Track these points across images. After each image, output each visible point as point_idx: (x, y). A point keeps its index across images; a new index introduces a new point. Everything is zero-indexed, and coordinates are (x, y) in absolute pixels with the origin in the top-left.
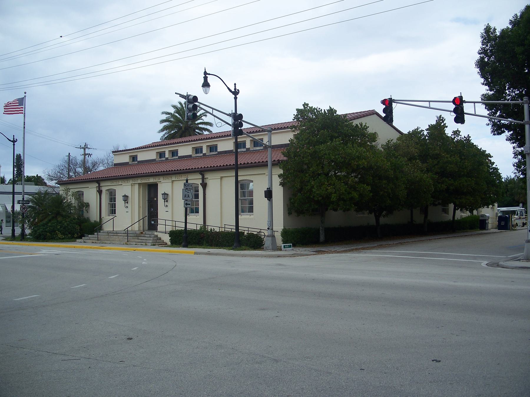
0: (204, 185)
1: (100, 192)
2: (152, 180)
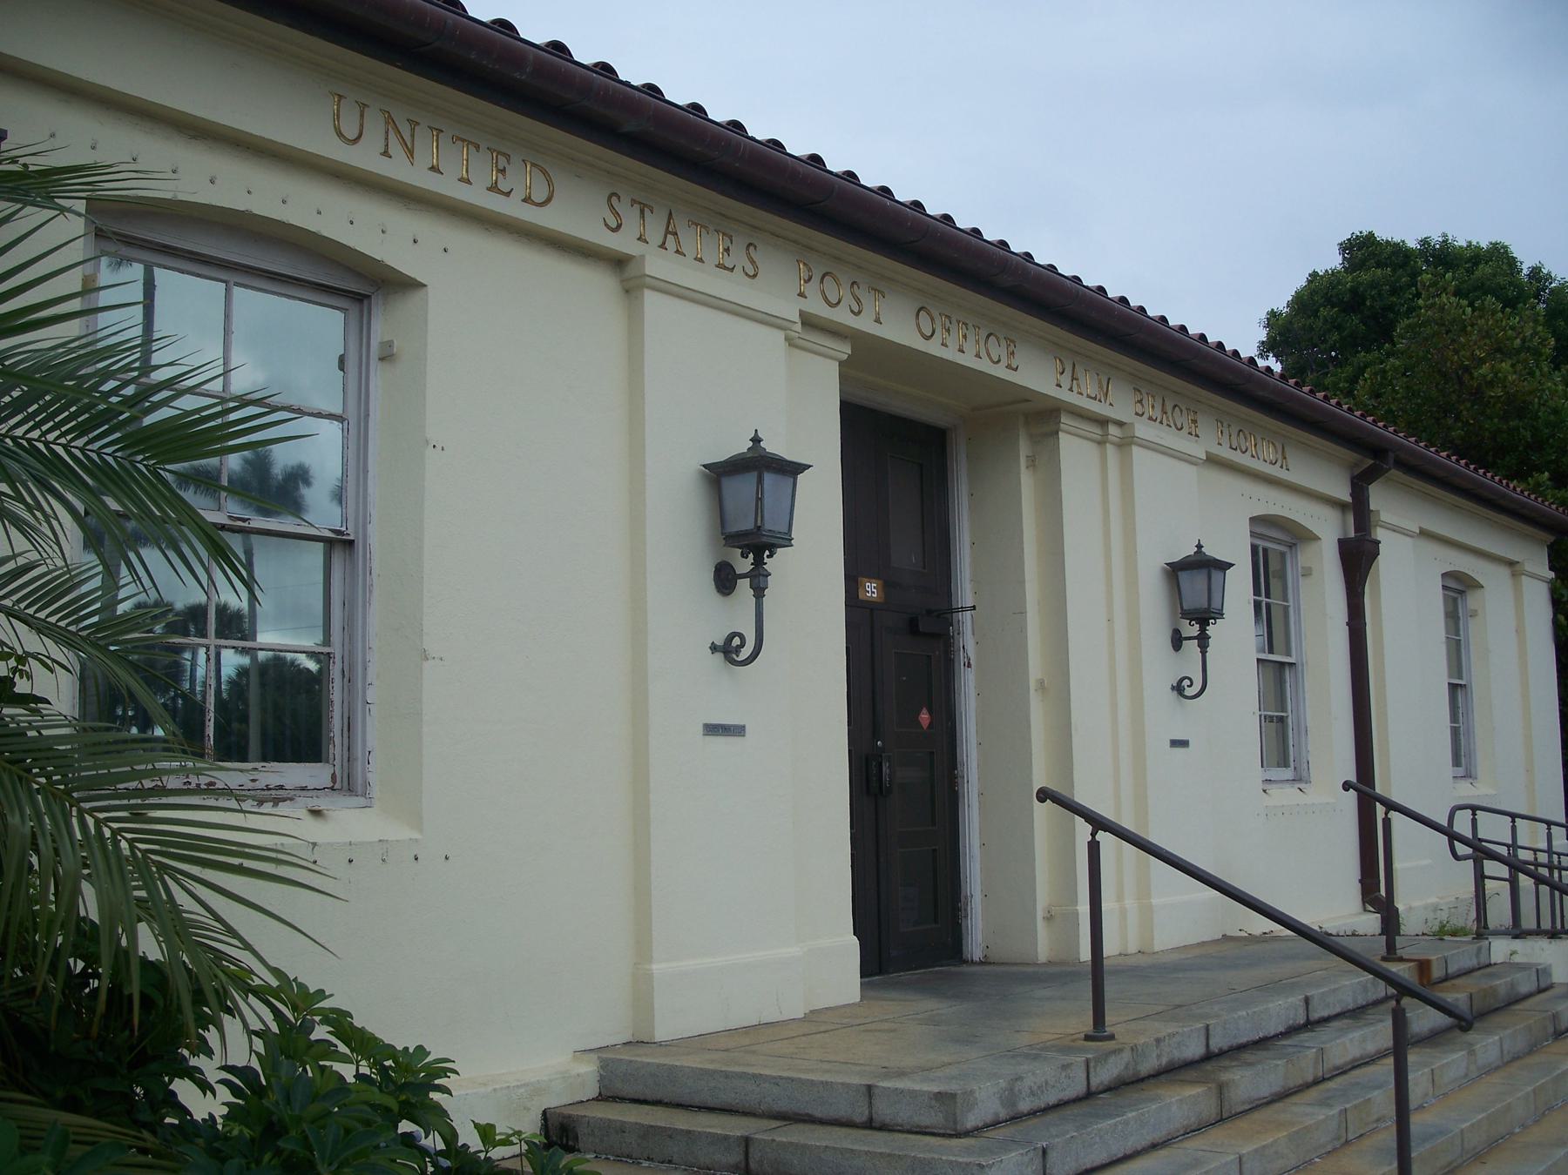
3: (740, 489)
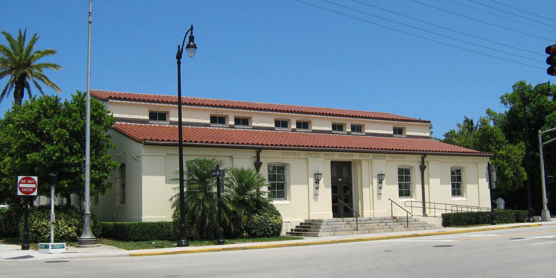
0: (423, 168)
2: (356, 157)
3: (380, 176)
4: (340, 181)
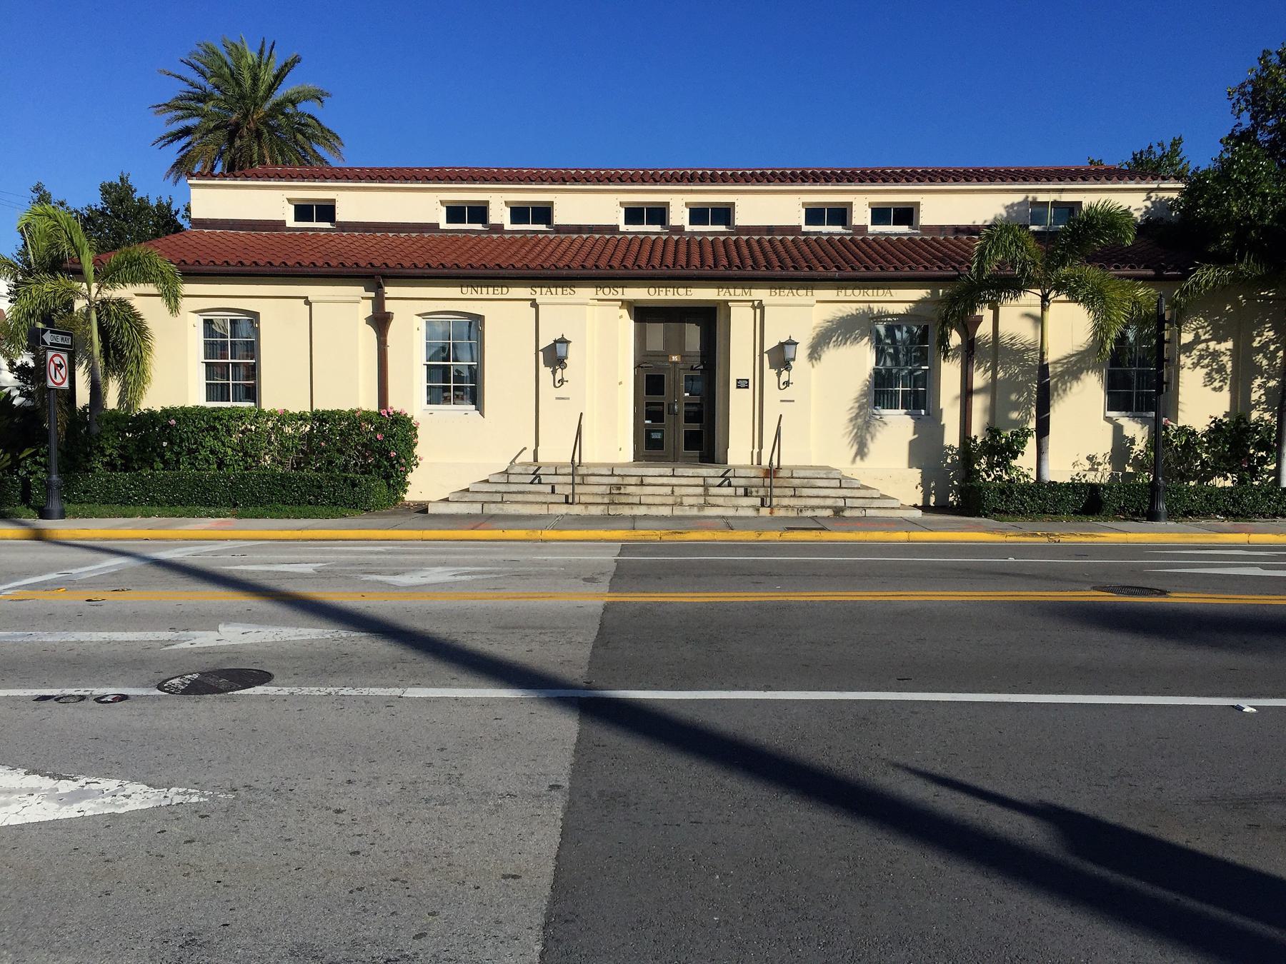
1: (380, 321)
4: (675, 363)
